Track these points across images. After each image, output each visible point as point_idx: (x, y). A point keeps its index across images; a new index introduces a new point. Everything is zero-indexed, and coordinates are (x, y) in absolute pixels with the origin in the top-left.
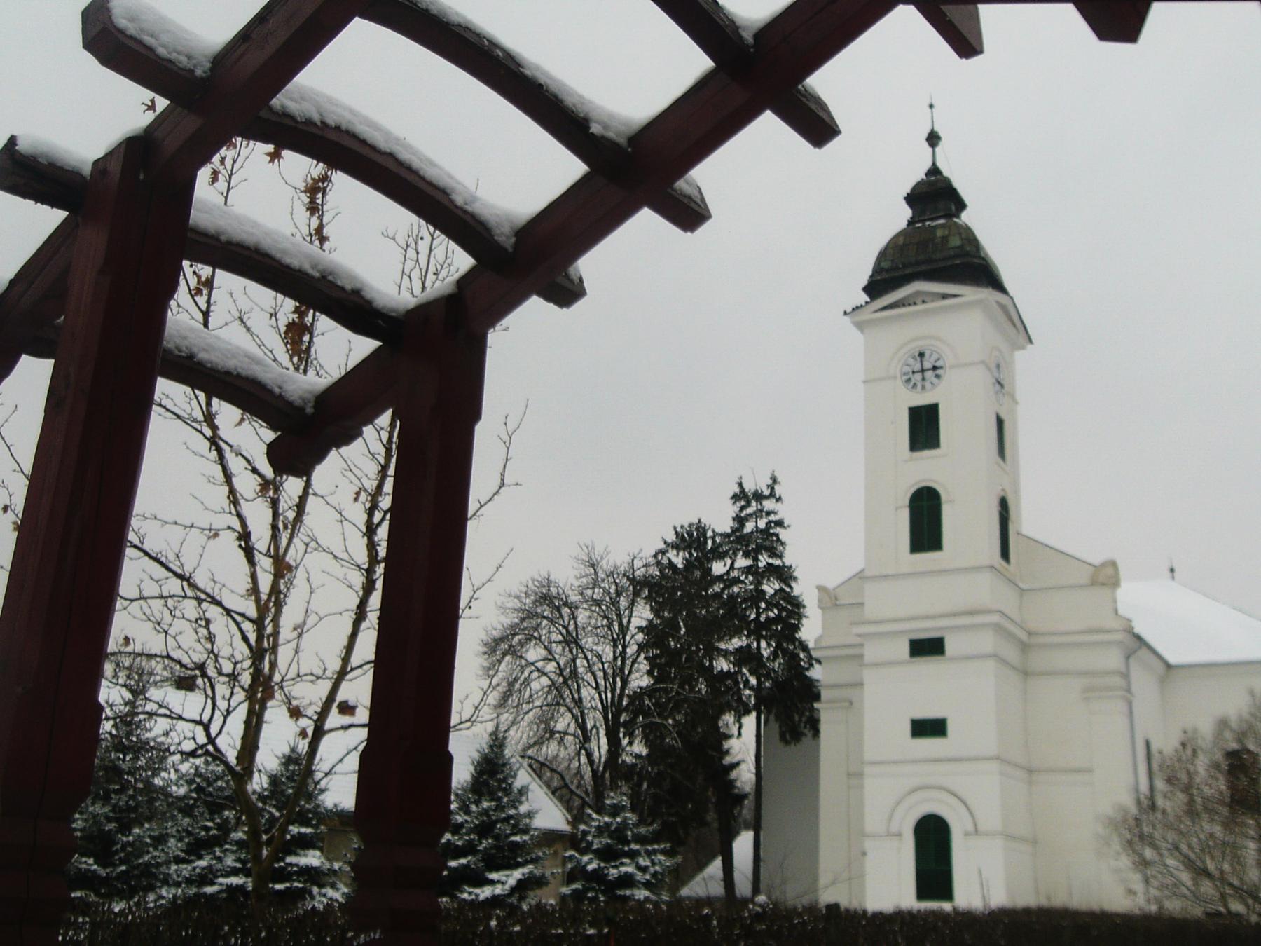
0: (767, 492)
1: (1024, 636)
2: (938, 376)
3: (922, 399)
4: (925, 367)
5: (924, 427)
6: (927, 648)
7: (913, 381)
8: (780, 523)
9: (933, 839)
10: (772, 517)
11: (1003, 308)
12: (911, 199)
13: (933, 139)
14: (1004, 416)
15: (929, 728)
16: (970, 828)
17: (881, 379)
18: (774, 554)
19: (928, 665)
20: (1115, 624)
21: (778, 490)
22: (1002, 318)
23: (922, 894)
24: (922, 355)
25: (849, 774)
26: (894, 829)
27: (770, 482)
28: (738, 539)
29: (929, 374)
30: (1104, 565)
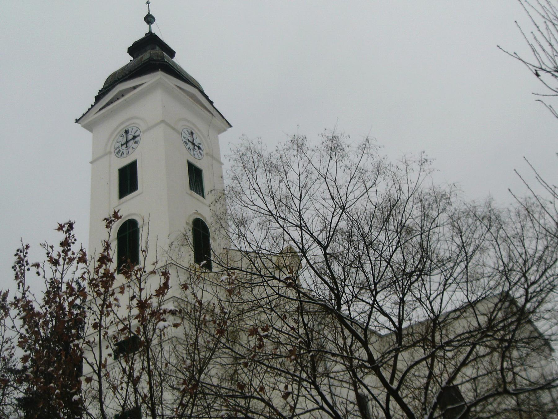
2: (136, 142)
3: (125, 161)
4: (129, 138)
5: (128, 180)
7: (122, 151)
11: (193, 96)
12: (132, 51)
13: (149, 19)
24: (127, 132)
25: (454, 184)
29: (131, 143)
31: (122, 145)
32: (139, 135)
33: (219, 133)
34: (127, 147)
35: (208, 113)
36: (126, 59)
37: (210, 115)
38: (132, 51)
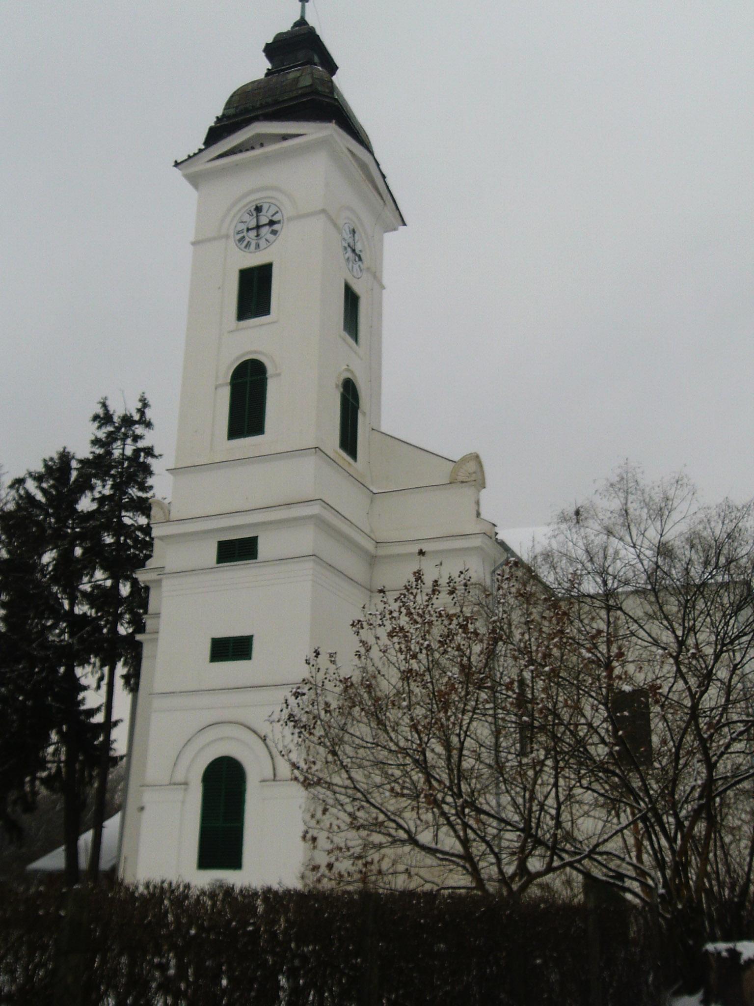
0: (136, 417)
1: (369, 546)
2: (274, 232)
4: (262, 222)
5: (255, 292)
6: (237, 550)
7: (247, 239)
8: (149, 452)
9: (224, 786)
10: (141, 444)
11: (363, 167)
12: (270, 51)
14: (358, 288)
15: (231, 649)
16: (269, 773)
17: (214, 239)
18: (143, 488)
19: (239, 573)
20: (472, 527)
21: (149, 414)
22: (358, 175)
23: (206, 861)
24: (258, 209)
26: (179, 777)
27: (140, 405)
28: (98, 466)
29: (265, 231)
30: (465, 460)
31: (248, 230)
32: (279, 222)
33: (386, 231)
34: (258, 235)
35: (378, 197)
36: (258, 67)
37: (381, 202)
38: (270, 51)
